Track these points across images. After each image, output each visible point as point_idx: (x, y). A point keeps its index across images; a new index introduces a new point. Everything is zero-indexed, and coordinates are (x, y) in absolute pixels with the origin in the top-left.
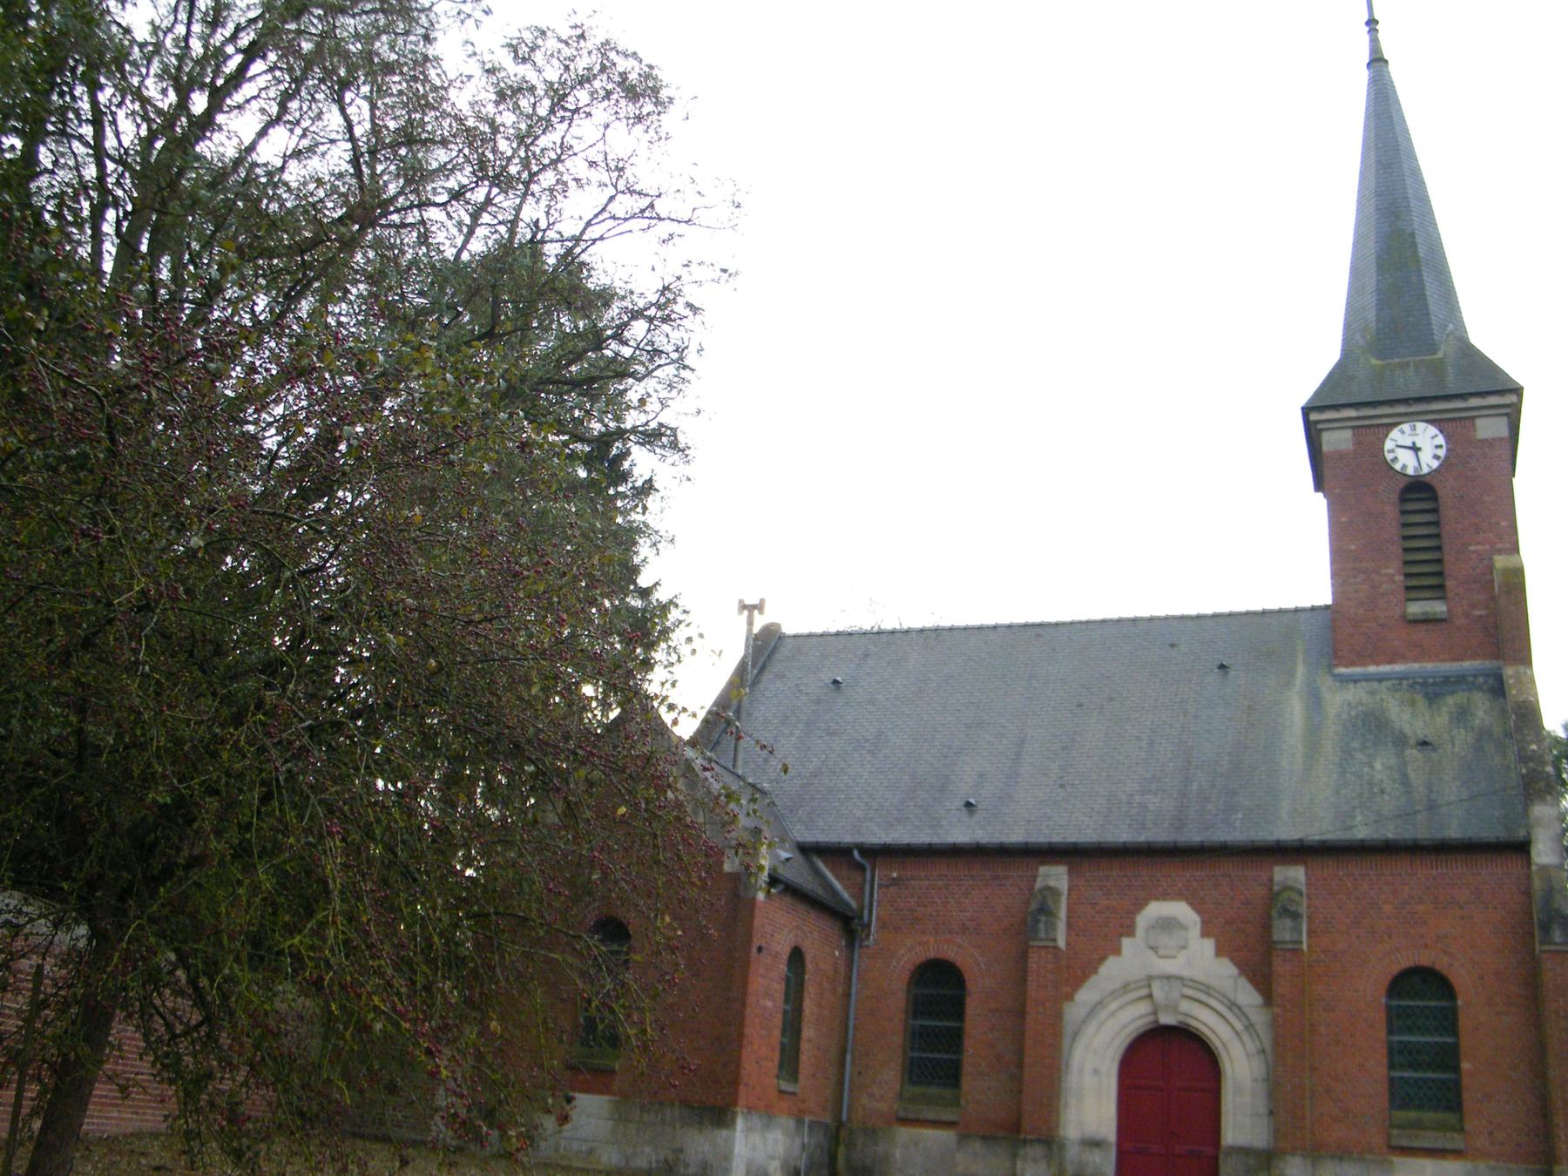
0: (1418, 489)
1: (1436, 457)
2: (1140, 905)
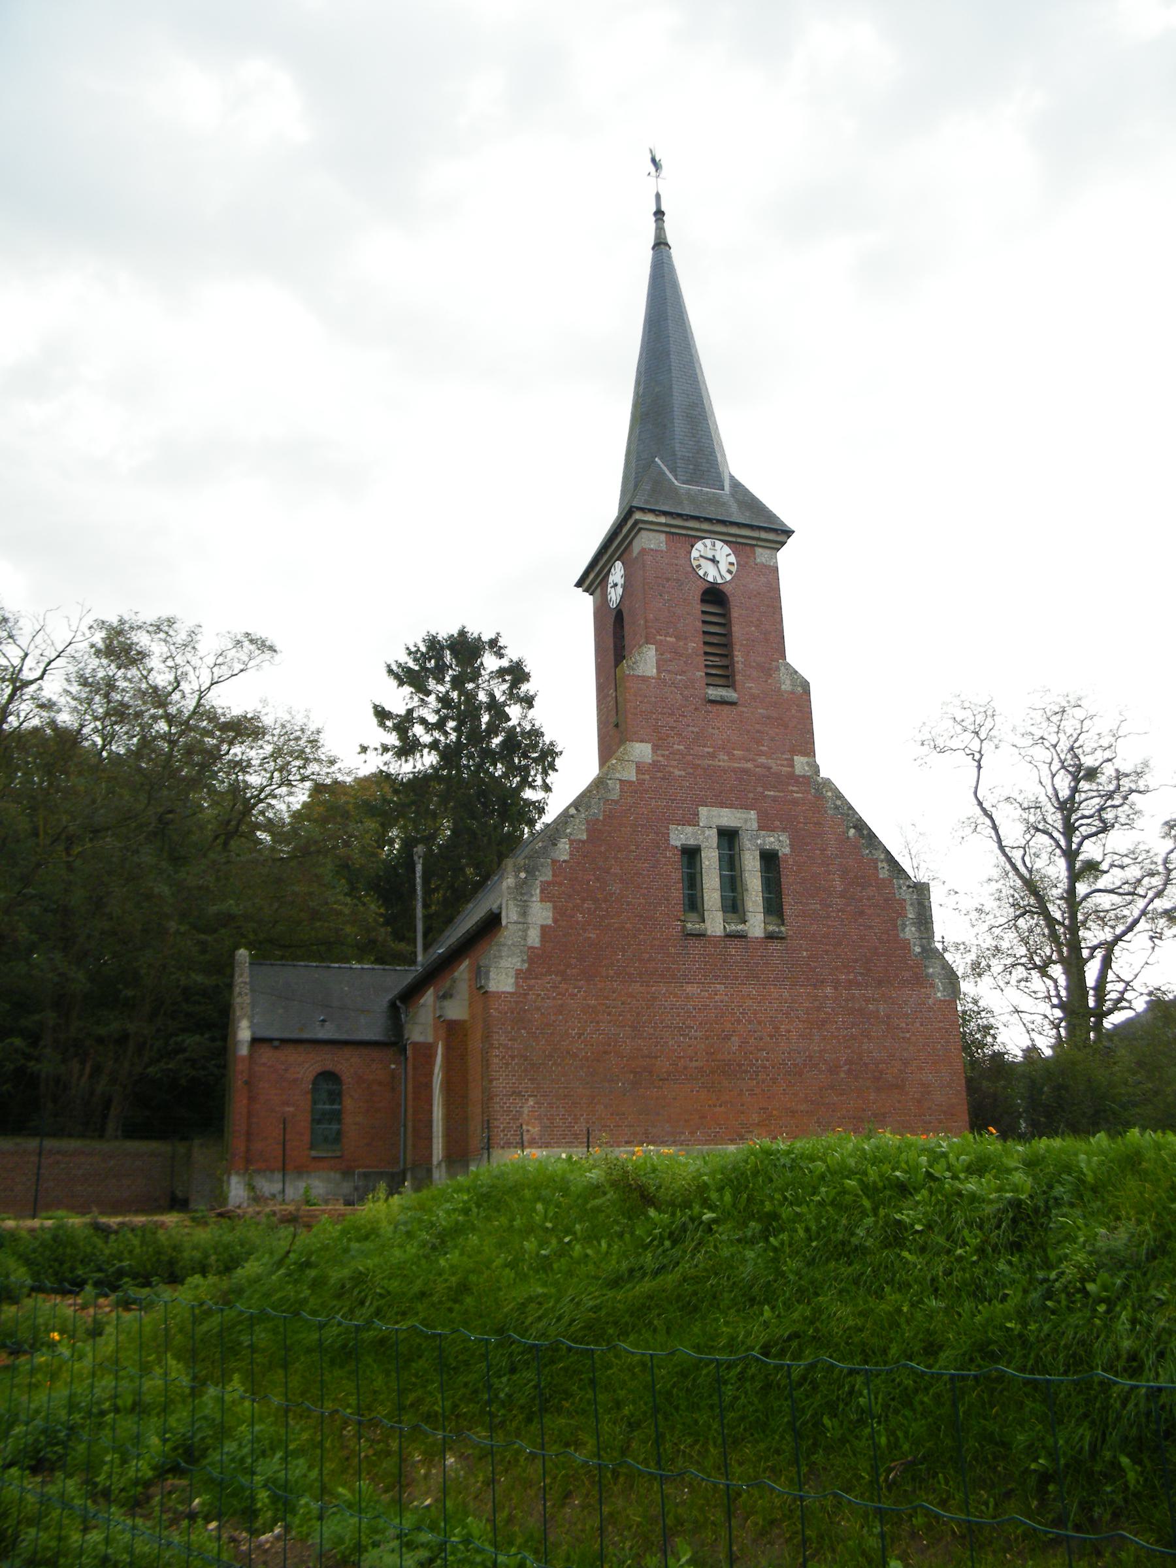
0: (714, 595)
1: (729, 572)
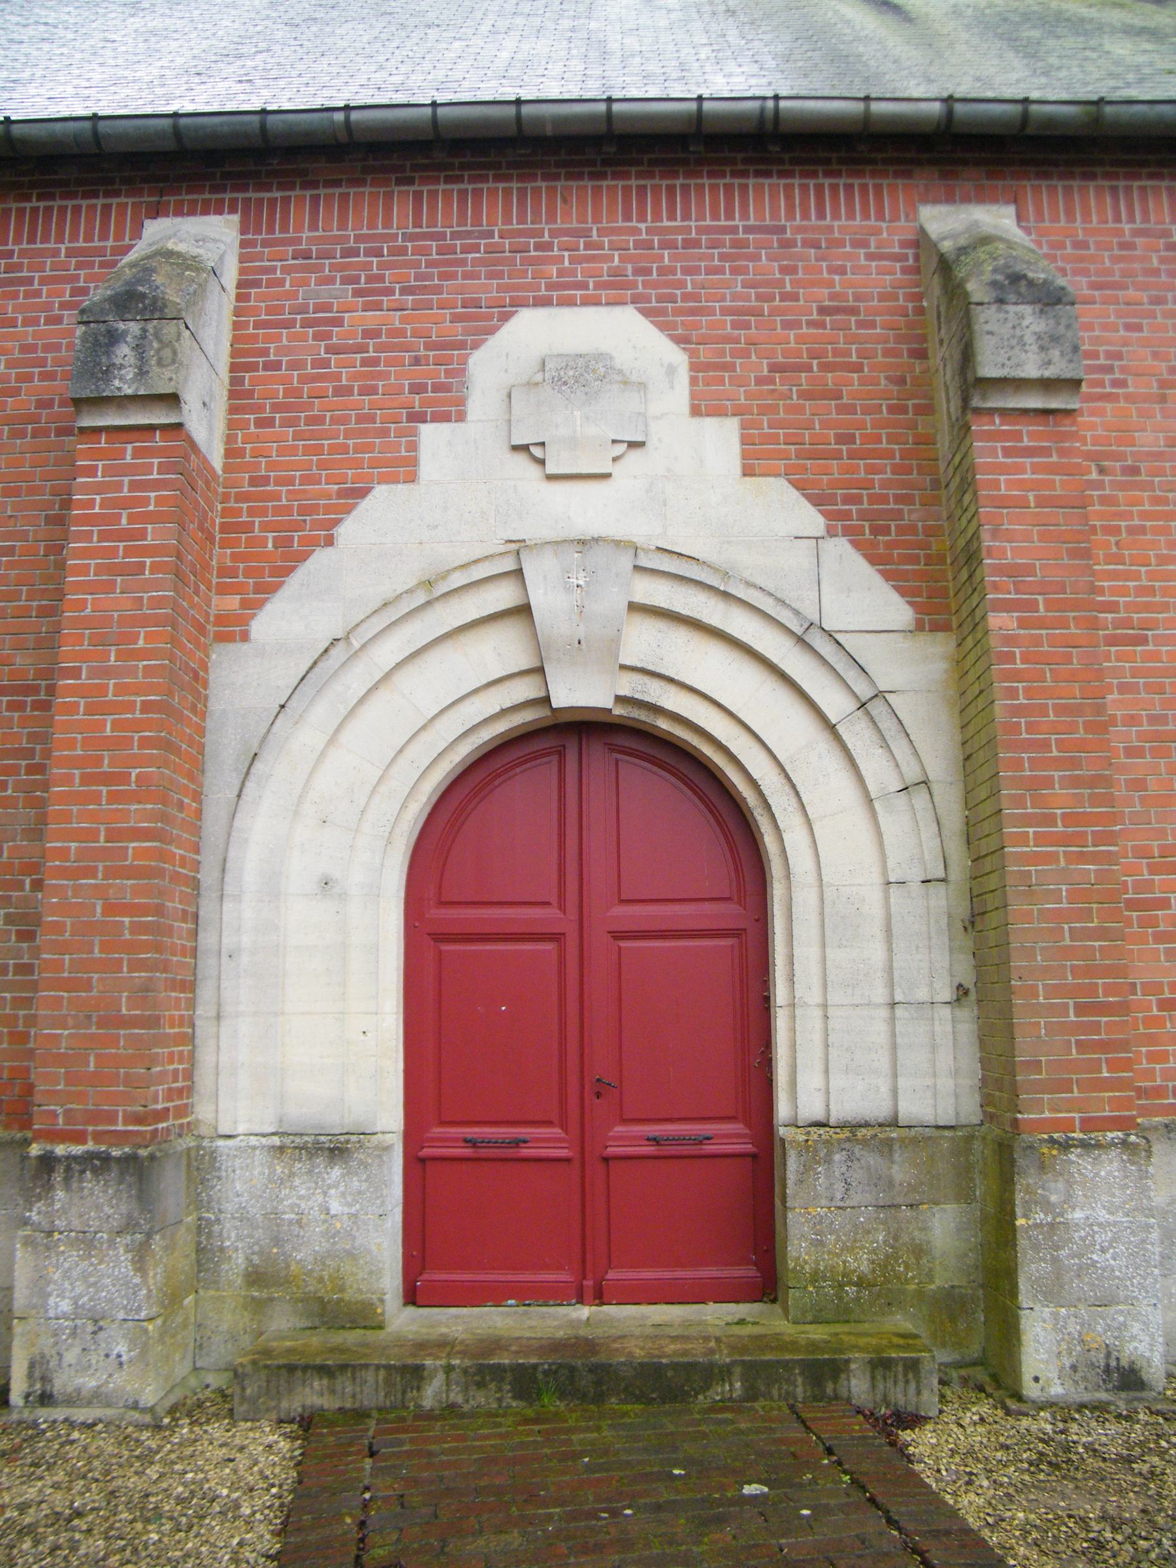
2: (483, 321)
